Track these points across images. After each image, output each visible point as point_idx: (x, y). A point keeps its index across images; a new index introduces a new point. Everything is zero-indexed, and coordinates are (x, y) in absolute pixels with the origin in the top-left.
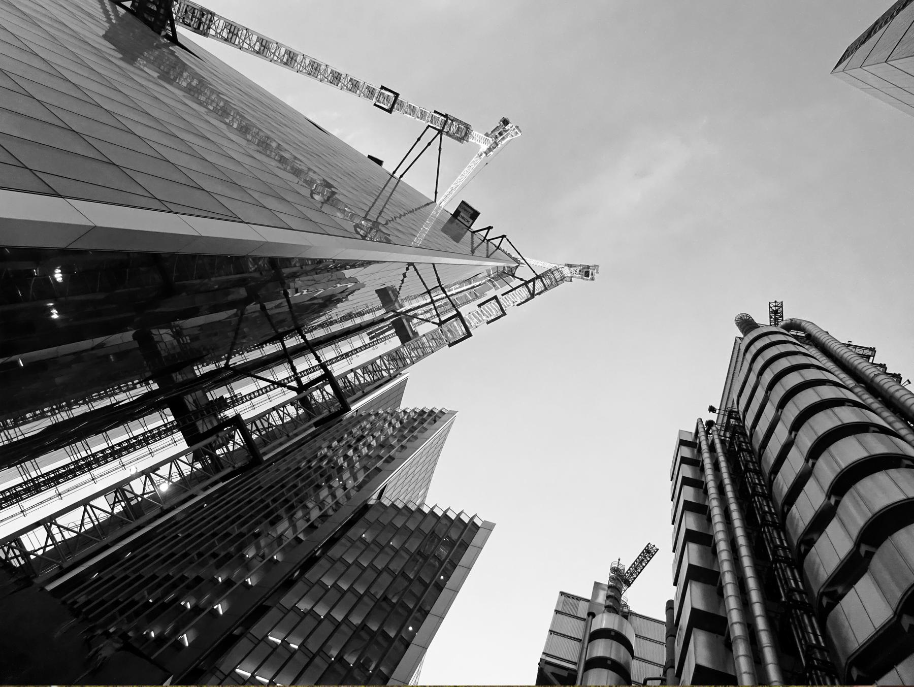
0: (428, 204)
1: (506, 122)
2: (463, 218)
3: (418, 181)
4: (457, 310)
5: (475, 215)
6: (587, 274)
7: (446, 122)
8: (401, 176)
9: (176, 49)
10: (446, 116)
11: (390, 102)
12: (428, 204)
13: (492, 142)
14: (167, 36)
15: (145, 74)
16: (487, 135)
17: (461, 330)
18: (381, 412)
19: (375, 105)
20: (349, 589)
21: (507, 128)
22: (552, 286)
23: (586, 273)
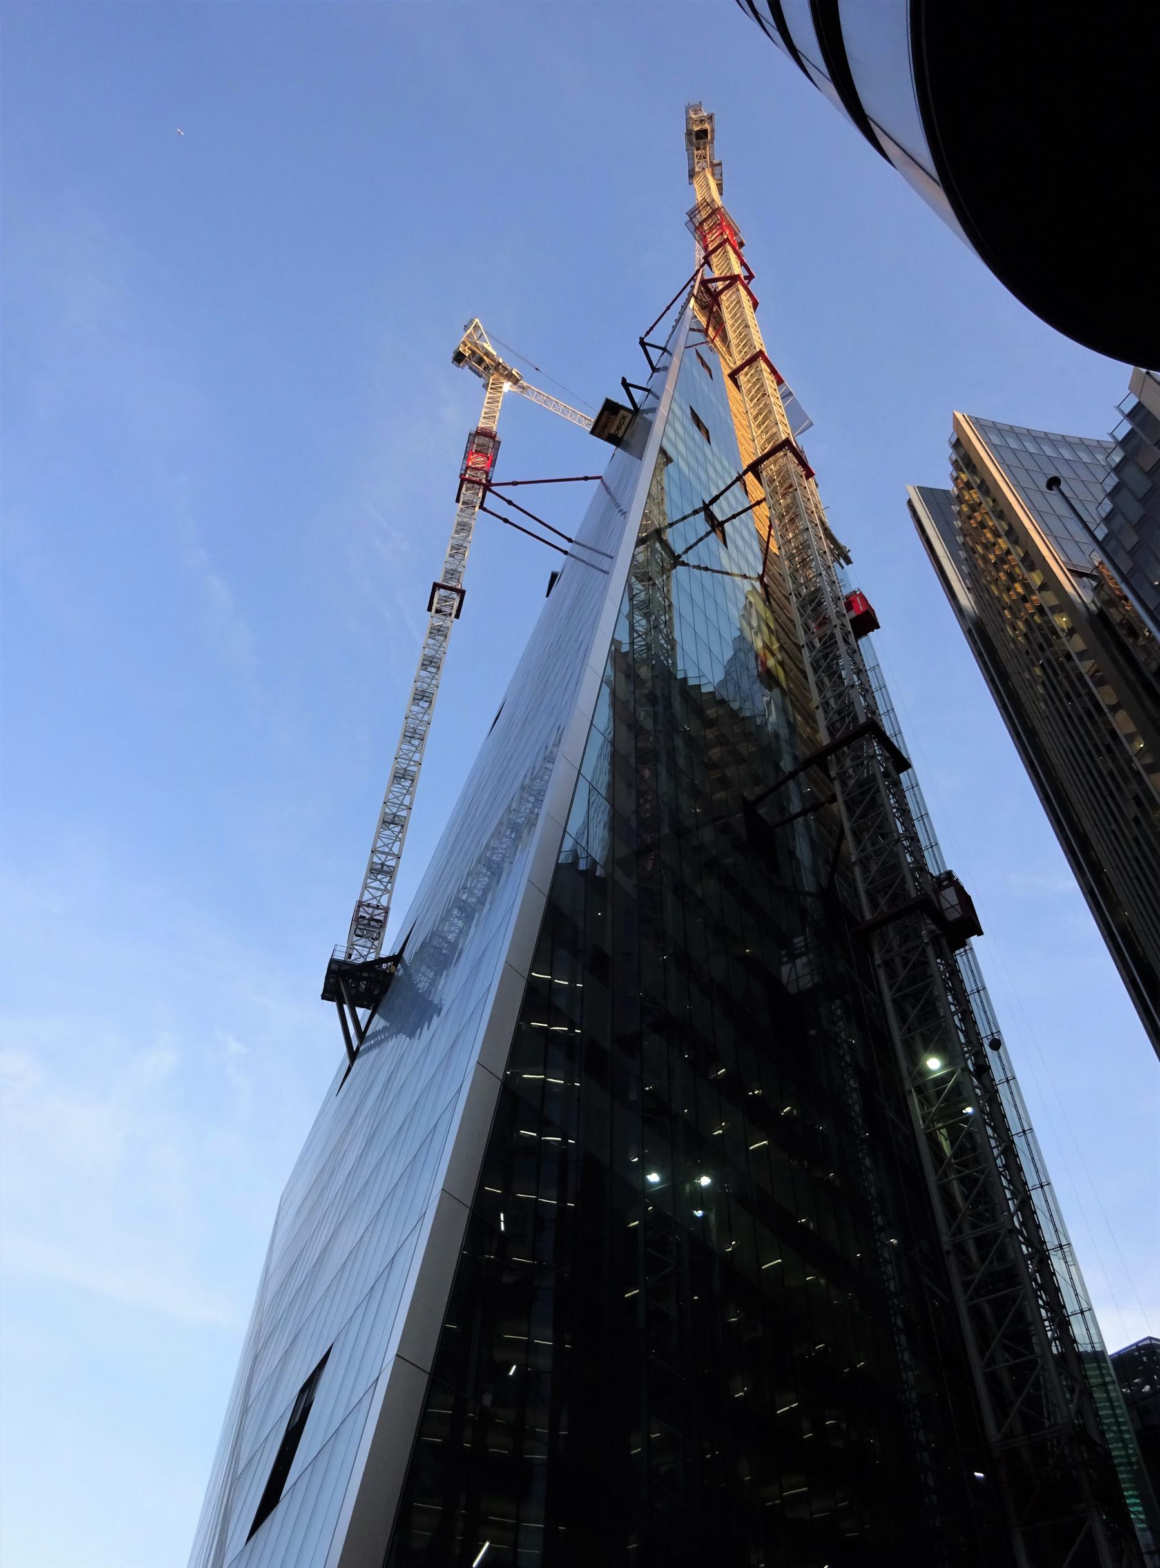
0: (607, 488)
1: (459, 358)
2: (619, 428)
3: (571, 509)
4: (745, 472)
5: (610, 408)
6: (702, 134)
7: (470, 481)
8: (570, 540)
9: (406, 956)
10: (463, 480)
11: (447, 596)
12: (607, 488)
14: (396, 965)
15: (449, 989)
16: (486, 386)
17: (787, 460)
19: (457, 616)
23: (699, 138)
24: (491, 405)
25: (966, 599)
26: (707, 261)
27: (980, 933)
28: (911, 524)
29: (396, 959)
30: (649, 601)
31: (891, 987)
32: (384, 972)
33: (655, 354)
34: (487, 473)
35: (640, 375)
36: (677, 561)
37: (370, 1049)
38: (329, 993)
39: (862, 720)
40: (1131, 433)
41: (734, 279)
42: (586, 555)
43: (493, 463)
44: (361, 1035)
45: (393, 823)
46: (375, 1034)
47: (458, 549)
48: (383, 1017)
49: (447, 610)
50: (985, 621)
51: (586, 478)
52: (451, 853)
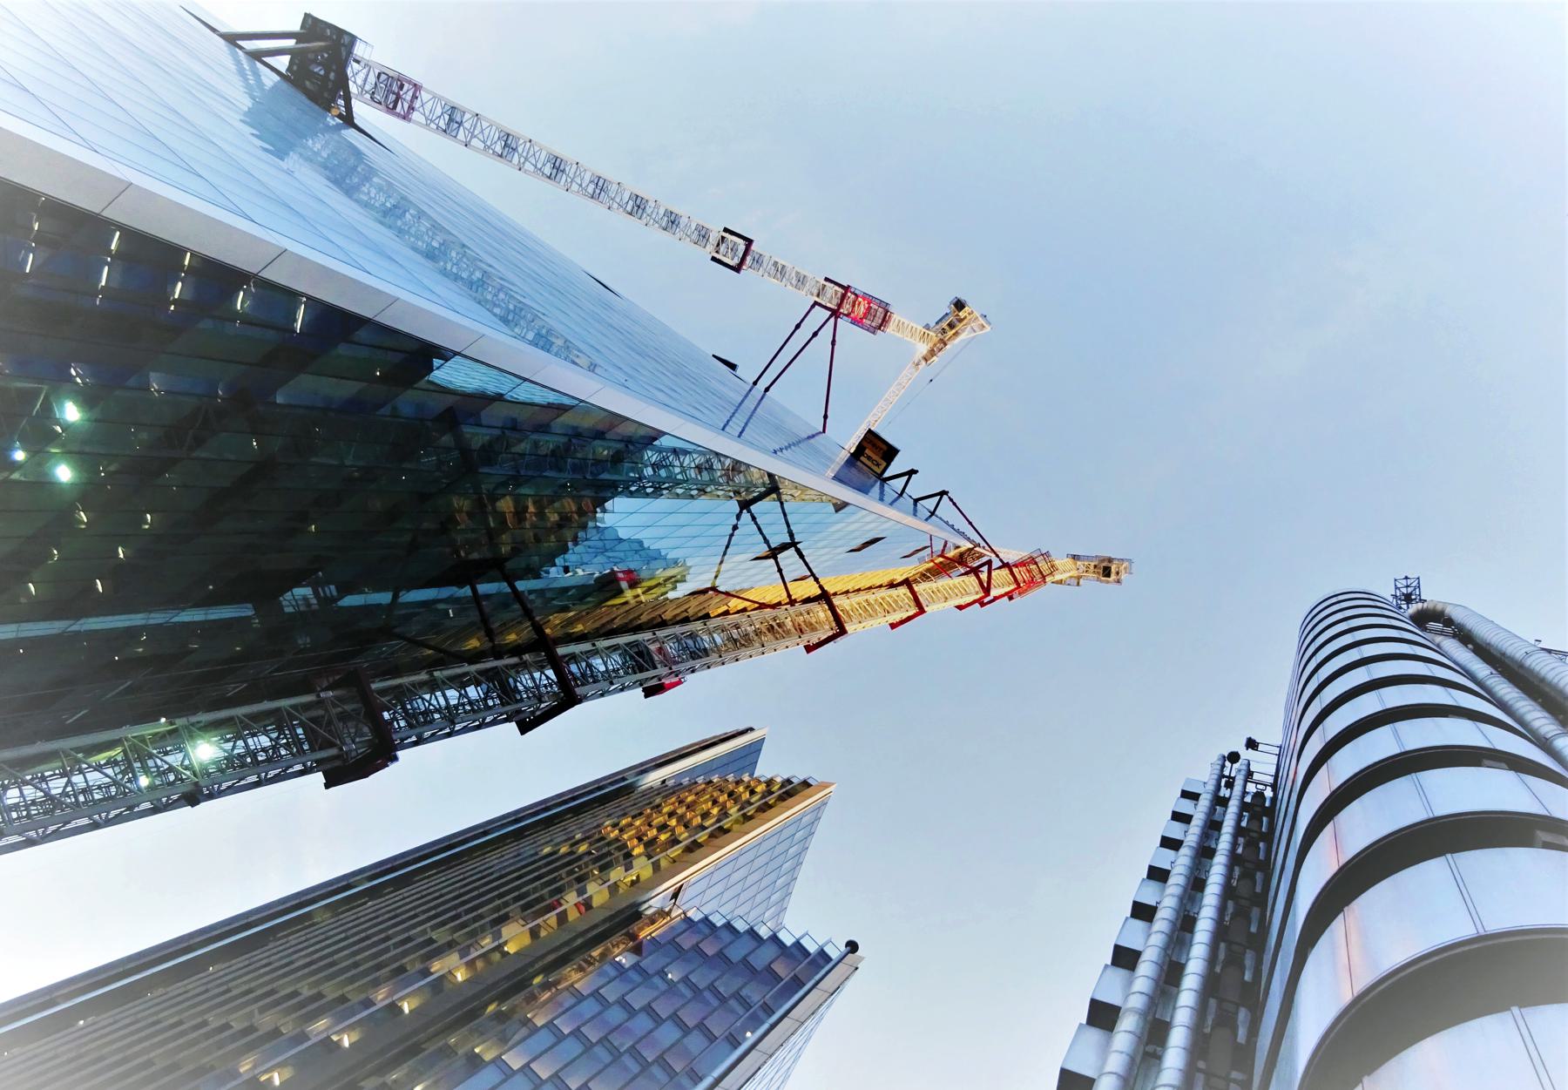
1: (959, 305)
2: (869, 458)
5: (890, 453)
6: (1107, 572)
7: (844, 296)
8: (767, 390)
9: (350, 134)
10: (847, 289)
11: (737, 253)
13: (935, 339)
14: (340, 116)
18: (715, 779)
19: (714, 259)
20: (521, 1069)
21: (962, 314)
22: (1032, 584)
24: (908, 331)
25: (653, 778)
26: (1005, 565)
27: (327, 786)
28: (730, 729)
29: (348, 120)
30: (715, 475)
31: (293, 707)
32: (334, 101)
33: (932, 502)
34: (848, 315)
35: (917, 488)
36: (745, 505)
37: (238, 62)
38: (313, 28)
39: (578, 691)
40: (806, 953)
41: (987, 591)
42: (750, 404)
43: (857, 322)
44: (257, 56)
45: (451, 120)
46: (256, 74)
47: (780, 271)
48: (275, 86)
49: (723, 248)
50: (634, 796)
51: (826, 417)
52: (472, 213)
